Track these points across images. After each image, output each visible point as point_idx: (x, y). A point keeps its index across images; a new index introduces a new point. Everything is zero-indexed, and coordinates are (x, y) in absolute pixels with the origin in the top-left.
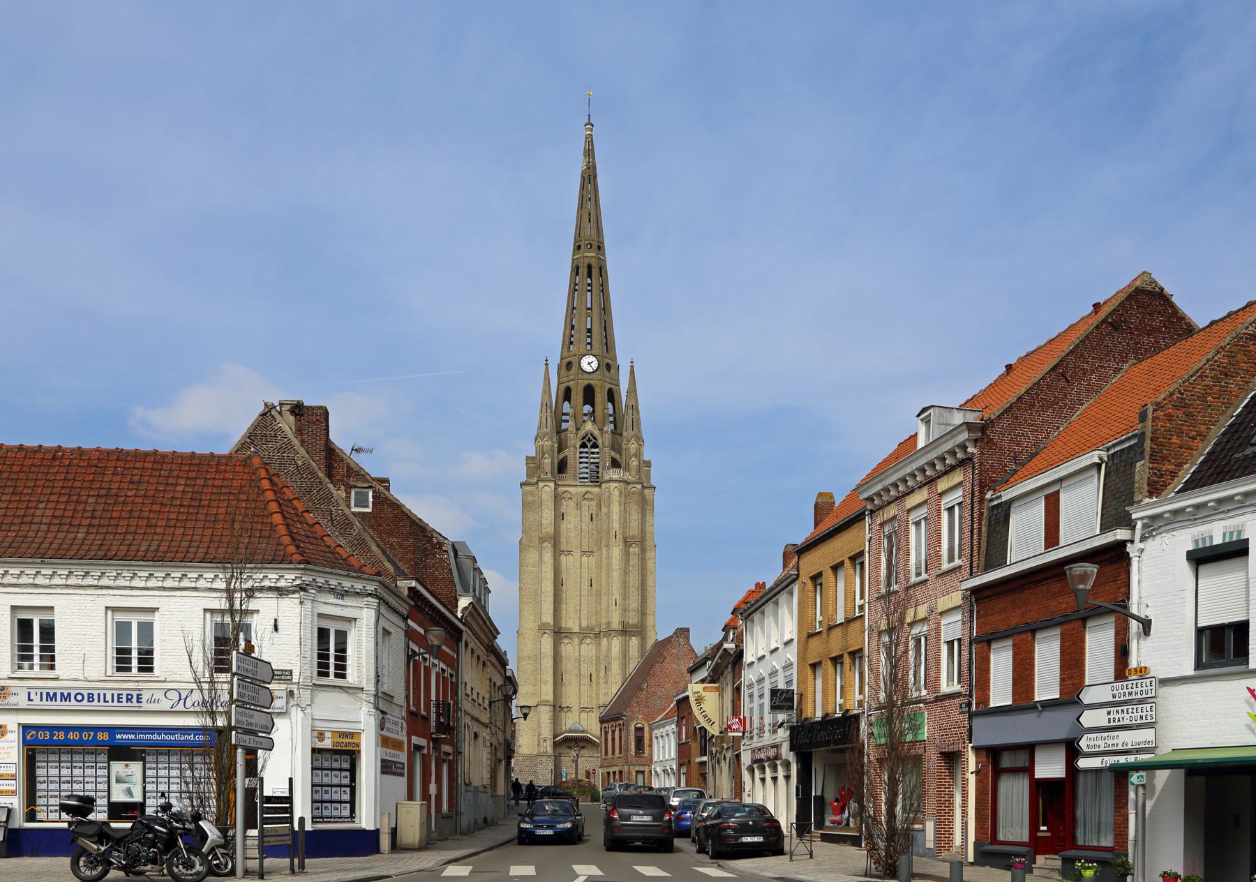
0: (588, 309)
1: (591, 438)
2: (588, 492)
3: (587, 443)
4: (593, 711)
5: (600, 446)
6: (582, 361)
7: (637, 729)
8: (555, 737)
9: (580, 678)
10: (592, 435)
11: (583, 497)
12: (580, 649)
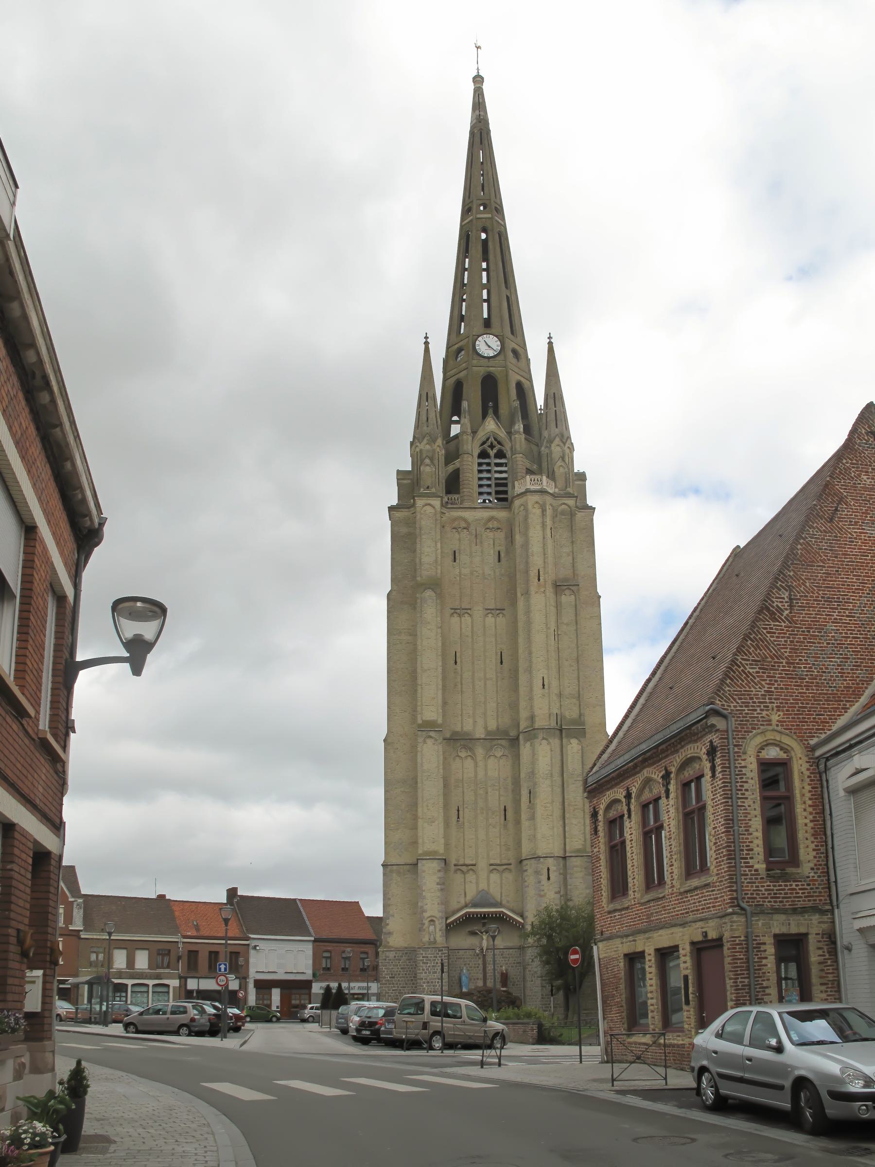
1: (495, 443)
3: (489, 450)
4: (510, 870)
5: (509, 454)
6: (477, 343)
7: (765, 766)
10: (495, 439)
11: (485, 524)
12: (486, 766)
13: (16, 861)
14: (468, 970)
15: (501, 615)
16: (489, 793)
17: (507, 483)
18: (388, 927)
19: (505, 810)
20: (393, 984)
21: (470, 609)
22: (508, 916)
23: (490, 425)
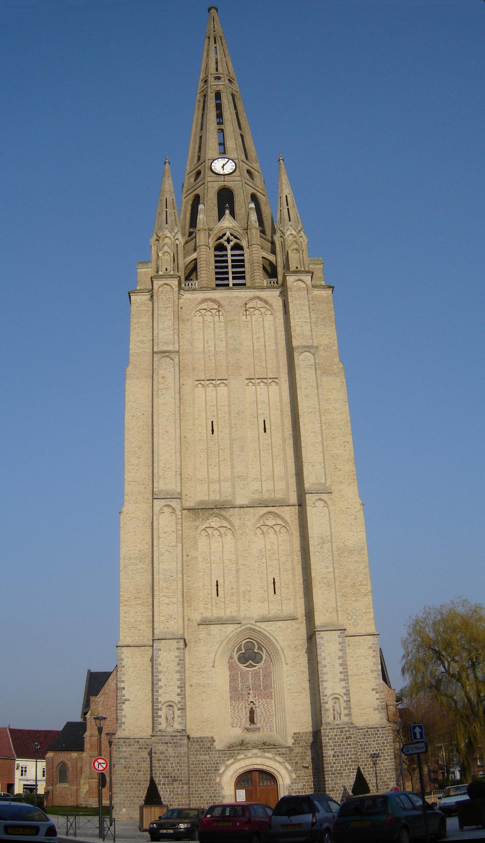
1: (231, 238)
13: (256, 278)
17: (244, 272)
21: (226, 380)
23: (227, 222)
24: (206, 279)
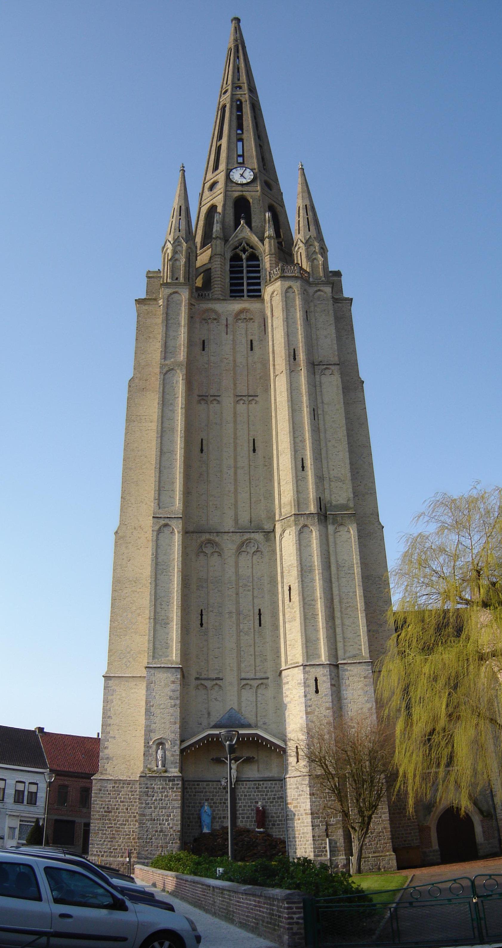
0: (239, 156)
1: (247, 247)
2: (247, 684)
3: (241, 254)
8: (182, 741)
9: (238, 619)
10: (248, 245)
14: (211, 807)
15: (254, 402)
16: (240, 595)
18: (106, 751)
19: (260, 614)
20: (110, 820)
21: (219, 396)
22: (263, 739)
24: (220, 289)
